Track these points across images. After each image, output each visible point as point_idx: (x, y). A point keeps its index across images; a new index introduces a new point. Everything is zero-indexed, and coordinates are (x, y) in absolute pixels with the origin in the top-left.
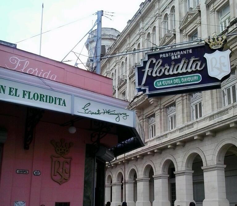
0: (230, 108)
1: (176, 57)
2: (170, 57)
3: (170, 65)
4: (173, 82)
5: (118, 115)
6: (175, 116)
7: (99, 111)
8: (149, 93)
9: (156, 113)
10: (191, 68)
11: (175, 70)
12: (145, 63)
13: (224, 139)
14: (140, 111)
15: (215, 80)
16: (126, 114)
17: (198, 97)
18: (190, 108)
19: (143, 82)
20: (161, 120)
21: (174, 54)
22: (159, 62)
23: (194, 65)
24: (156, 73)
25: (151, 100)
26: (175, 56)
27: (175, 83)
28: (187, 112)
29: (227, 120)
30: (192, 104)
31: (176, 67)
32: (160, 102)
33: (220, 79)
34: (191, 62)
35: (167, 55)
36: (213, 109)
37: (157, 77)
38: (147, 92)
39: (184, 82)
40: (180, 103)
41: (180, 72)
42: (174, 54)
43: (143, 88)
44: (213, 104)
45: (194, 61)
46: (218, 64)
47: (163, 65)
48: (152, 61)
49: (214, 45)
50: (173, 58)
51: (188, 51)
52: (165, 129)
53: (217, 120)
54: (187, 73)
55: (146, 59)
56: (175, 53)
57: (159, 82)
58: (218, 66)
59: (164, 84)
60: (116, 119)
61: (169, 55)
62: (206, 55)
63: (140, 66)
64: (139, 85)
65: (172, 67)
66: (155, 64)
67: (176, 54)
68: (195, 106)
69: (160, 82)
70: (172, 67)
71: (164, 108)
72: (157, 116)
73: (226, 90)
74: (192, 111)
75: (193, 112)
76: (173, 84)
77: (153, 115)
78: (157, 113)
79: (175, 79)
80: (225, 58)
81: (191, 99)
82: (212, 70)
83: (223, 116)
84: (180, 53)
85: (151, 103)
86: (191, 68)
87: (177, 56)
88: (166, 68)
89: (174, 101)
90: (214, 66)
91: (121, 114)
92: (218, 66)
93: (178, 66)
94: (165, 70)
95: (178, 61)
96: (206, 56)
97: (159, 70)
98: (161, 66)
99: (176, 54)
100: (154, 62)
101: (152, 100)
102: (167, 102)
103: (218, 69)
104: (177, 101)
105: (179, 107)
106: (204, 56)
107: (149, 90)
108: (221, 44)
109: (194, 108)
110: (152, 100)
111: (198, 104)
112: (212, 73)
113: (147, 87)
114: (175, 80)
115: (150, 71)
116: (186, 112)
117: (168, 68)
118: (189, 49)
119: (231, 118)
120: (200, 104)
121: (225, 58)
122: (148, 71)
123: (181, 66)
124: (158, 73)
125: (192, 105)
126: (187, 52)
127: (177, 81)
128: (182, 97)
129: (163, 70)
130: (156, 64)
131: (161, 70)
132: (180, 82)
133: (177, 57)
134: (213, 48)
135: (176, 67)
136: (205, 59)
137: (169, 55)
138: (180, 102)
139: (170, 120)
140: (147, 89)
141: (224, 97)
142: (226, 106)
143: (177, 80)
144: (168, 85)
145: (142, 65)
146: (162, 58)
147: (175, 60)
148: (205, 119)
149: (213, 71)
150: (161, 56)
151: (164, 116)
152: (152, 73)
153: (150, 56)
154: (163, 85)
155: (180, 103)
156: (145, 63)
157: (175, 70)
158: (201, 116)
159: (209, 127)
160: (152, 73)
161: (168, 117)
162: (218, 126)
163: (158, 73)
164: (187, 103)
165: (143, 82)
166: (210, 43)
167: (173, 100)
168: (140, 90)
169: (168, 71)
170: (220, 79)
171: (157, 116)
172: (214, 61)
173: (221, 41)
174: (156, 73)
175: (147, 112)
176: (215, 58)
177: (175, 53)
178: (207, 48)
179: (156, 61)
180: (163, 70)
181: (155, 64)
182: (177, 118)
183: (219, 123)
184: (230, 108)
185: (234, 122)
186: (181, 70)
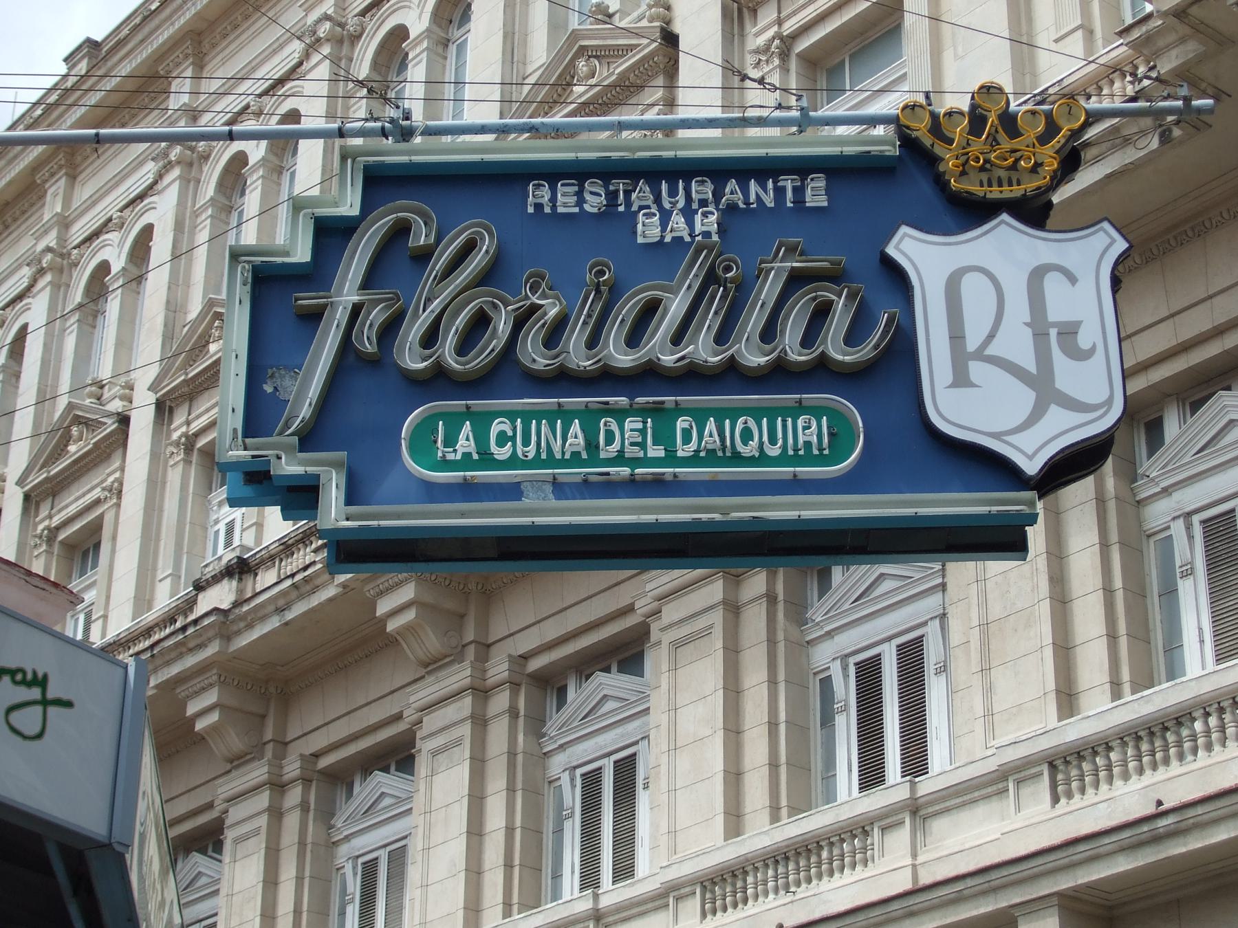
0: (886, 820)
4: (592, 446)
6: (398, 858)
9: (235, 814)
10: (769, 333)
14: (450, 604)
15: (985, 465)
17: (610, 705)
20: (271, 881)
22: (469, 248)
24: (430, 338)
25: (398, 598)
31: (628, 309)
32: (282, 727)
33: (1031, 467)
34: (769, 290)
36: (734, 822)
37: (437, 381)
38: (334, 510)
43: (290, 467)
44: (734, 777)
45: (796, 280)
46: (1012, 329)
48: (401, 231)
49: (982, 169)
51: (788, 183)
52: (802, 780)
53: (1122, 798)
54: (731, 375)
55: (350, 205)
60: (25, 737)
63: (279, 260)
66: (423, 257)
69: (467, 427)
71: (306, 781)
72: (435, 753)
73: (1189, 527)
74: (548, 827)
75: (559, 831)
77: (399, 756)
78: (246, 819)
79: (620, 414)
80: (1073, 279)
81: (817, 612)
82: (961, 379)
83: (826, 884)
85: (200, 725)
86: (769, 333)
87: (688, 214)
88: (534, 308)
89: (401, 727)
90: (972, 344)
92: (1016, 343)
93: (651, 309)
96: (912, 249)
97: (461, 320)
98: (486, 278)
100: (421, 237)
101: (407, 593)
102: (552, 631)
104: (235, 814)
105: (443, 785)
107: (352, 497)
108: (1038, 165)
109: (568, 801)
110: (407, 593)
111: (383, 855)
112: (962, 407)
113: (336, 465)
114: (614, 427)
115: (377, 316)
120: (626, 771)
122: (356, 310)
123: (676, 306)
127: (627, 432)
128: (735, 581)
129: (502, 325)
131: (481, 322)
135: (628, 309)
136: (897, 277)
138: (701, 623)
139: (354, 887)
141: (827, 720)
142: (566, 896)
143: (632, 424)
145: (302, 253)
149: (970, 384)
151: (302, 844)
153: (380, 182)
154: (487, 460)
156: (331, 234)
158: (624, 870)
159: (1191, 813)
161: (333, 856)
164: (512, 754)
167: (398, 717)
168: (258, 484)
169: (555, 334)
170: (1031, 467)
171: (435, 753)
172: (976, 293)
173: (1044, 139)
175: (331, 723)
178: (954, 172)
180: (502, 325)
182: (413, 874)
184: (886, 820)
186: (677, 339)
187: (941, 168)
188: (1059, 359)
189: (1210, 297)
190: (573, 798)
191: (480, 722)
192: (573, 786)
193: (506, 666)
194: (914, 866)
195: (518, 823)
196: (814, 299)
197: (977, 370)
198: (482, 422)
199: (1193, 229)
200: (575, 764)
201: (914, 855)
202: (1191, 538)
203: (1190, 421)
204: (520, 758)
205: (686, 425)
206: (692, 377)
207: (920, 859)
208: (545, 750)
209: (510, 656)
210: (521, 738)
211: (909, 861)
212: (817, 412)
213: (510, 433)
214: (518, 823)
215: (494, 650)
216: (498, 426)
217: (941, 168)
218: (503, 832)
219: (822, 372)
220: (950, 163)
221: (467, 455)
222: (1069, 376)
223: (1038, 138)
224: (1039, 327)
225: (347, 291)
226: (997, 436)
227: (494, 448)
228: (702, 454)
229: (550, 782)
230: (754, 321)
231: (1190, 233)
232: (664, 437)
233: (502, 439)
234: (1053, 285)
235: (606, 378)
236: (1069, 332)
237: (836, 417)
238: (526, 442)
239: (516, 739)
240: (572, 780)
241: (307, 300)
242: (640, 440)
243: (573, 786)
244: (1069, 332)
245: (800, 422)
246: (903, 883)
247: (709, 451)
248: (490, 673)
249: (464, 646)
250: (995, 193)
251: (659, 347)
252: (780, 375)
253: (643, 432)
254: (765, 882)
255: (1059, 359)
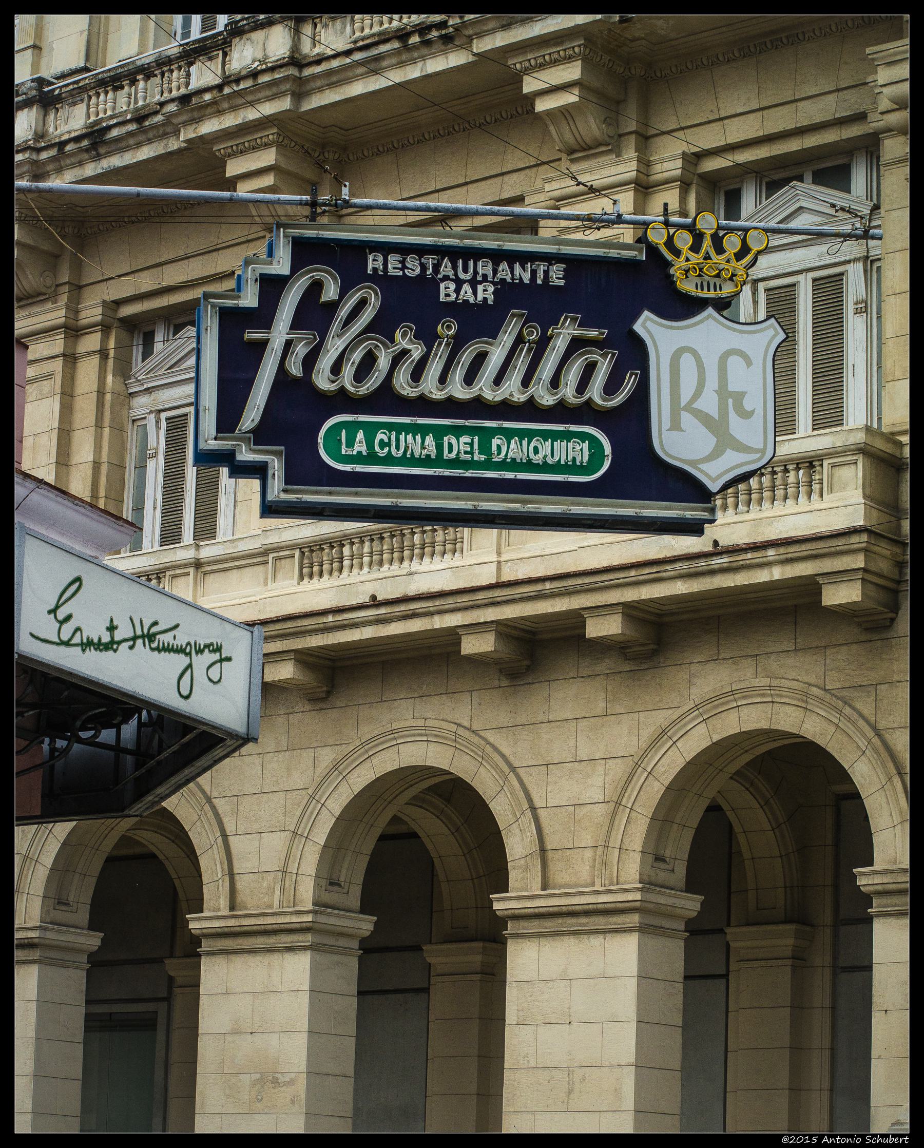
1: (466, 287)
2: (427, 285)
3: (428, 337)
5: (189, 654)
7: (112, 628)
8: (284, 496)
10: (555, 383)
11: (458, 374)
12: (272, 287)
13: (393, 732)
16: (219, 649)
18: (119, 430)
19: (252, 416)
21: (455, 267)
22: (363, 303)
23: (565, 368)
24: (336, 369)
26: (459, 283)
27: (453, 455)
28: (96, 465)
29: (448, 602)
30: (141, 405)
31: (466, 357)
34: (560, 344)
35: (413, 268)
37: (343, 401)
39: (503, 465)
40: (49, 376)
41: (489, 395)
42: (455, 267)
43: (245, 455)
45: (576, 344)
47: (382, 327)
48: (316, 287)
50: (447, 291)
51: (542, 268)
54: (530, 410)
56: (460, 263)
57: (352, 428)
58: (709, 403)
59: (383, 453)
61: (424, 267)
62: (648, 324)
64: (219, 429)
65: (441, 352)
66: (333, 307)
67: (465, 270)
68: (163, 425)
69: (360, 435)
70: (441, 352)
75: (141, 468)
76: (438, 461)
79: (458, 431)
80: (749, 362)
82: (676, 425)
84: (495, 272)
86: (555, 383)
87: (474, 283)
88: (405, 352)
90: (686, 395)
91: (200, 651)
92: (709, 403)
93: (481, 358)
94: (399, 358)
95: (479, 322)
96: (647, 325)
99: (465, 270)
100: (331, 292)
102: (146, 282)
103: (705, 419)
106: (638, 327)
107: (291, 478)
109: (152, 442)
112: (677, 441)
113: (277, 454)
115: (301, 350)
116: (91, 458)
117: (417, 352)
118: (550, 258)
119: (480, 596)
121: (749, 362)
122: (288, 344)
124: (348, 371)
125: (137, 412)
126: (534, 273)
130: (344, 312)
131: (369, 360)
132: (483, 457)
133: (475, 293)
134: (688, 287)
135: (466, 357)
137: (424, 267)
140: (277, 466)
143: (465, 439)
144: (405, 461)
146: (382, 280)
147: (458, 309)
148: (265, 553)
150: (374, 262)
152: (310, 361)
154: (372, 458)
155: (49, 376)
156: (272, 287)
157: (458, 374)
160: (310, 361)
162: (367, 633)
163: (348, 371)
164: (101, 393)
165: (252, 416)
166: (677, 253)
169: (417, 374)
172: (687, 363)
174: (336, 369)
176: (695, 353)
177: (460, 263)
179: (343, 293)
181: (333, 307)
183: (383, 610)
185: (497, 623)
187: (672, 271)
188: (732, 416)
189: (796, 101)
190: (158, 439)
191: (70, 359)
192: (158, 428)
193: (100, 310)
194: (499, 563)
195: (105, 457)
196: (586, 359)
197: (686, 417)
198: (371, 430)
199: (787, 37)
200: (161, 407)
201: (499, 553)
202: (755, 302)
203: (764, 203)
204: (108, 397)
205: (499, 442)
206: (505, 410)
207: (504, 558)
208: (131, 391)
209: (104, 302)
210: (110, 378)
211: (494, 558)
212: (583, 437)
213: (386, 440)
214: (105, 457)
215: (87, 292)
216: (380, 436)
217: (672, 271)
218: (90, 465)
219: (585, 413)
220: (676, 271)
221: (360, 453)
222: (737, 427)
223: (735, 254)
224: (723, 392)
225: (280, 331)
226: (693, 463)
227: (377, 449)
228: (508, 460)
229: (134, 421)
230: (547, 369)
231: (785, 41)
232: (485, 448)
233: (382, 444)
234: (734, 362)
235: (450, 407)
236: (739, 397)
237: (594, 443)
238: (398, 448)
239: (105, 378)
240: (158, 422)
241: (251, 335)
242: (469, 449)
243: (158, 428)
244: (739, 397)
245: (480, 264)
246: (487, 576)
247: (514, 460)
248: (83, 314)
249: (57, 286)
250: (704, 294)
251: (484, 387)
252: (562, 412)
253: (471, 444)
254: (361, 556)
255: (732, 416)
